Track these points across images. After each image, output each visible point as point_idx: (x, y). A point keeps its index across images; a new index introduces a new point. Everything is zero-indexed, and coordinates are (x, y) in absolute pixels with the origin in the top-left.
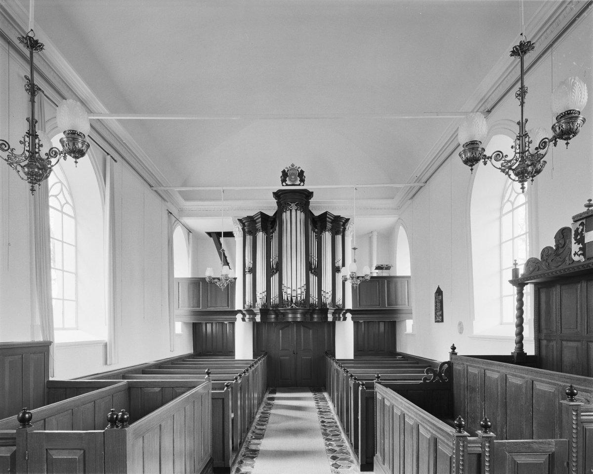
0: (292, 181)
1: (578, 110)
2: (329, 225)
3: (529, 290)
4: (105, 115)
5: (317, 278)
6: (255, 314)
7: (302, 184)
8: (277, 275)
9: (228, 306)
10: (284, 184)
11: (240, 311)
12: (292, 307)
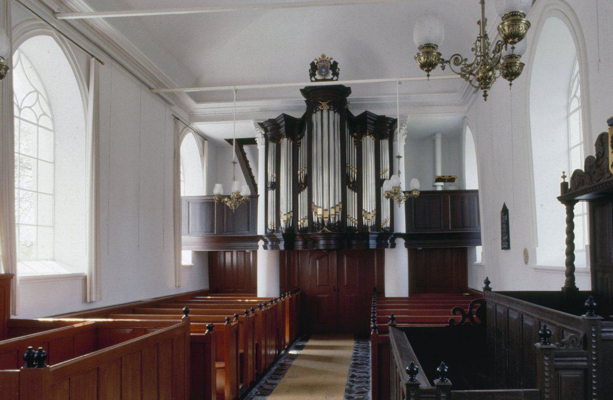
0: (322, 75)
1: (521, 12)
2: (370, 128)
3: (581, 208)
4: (91, 14)
5: (356, 194)
6: (278, 241)
7: (335, 78)
8: (306, 191)
9: (248, 230)
10: (313, 79)
11: (261, 237)
12: (324, 231)
